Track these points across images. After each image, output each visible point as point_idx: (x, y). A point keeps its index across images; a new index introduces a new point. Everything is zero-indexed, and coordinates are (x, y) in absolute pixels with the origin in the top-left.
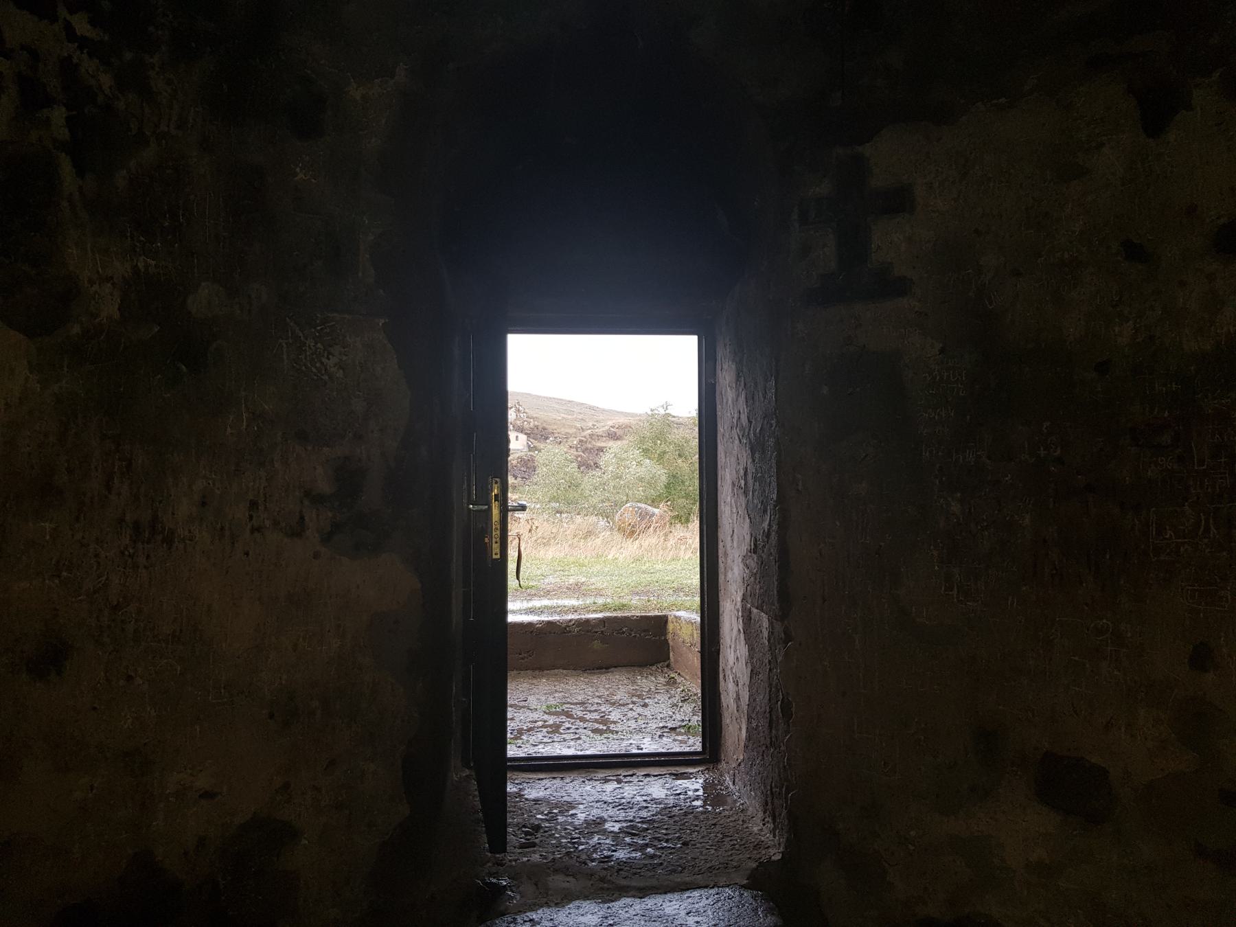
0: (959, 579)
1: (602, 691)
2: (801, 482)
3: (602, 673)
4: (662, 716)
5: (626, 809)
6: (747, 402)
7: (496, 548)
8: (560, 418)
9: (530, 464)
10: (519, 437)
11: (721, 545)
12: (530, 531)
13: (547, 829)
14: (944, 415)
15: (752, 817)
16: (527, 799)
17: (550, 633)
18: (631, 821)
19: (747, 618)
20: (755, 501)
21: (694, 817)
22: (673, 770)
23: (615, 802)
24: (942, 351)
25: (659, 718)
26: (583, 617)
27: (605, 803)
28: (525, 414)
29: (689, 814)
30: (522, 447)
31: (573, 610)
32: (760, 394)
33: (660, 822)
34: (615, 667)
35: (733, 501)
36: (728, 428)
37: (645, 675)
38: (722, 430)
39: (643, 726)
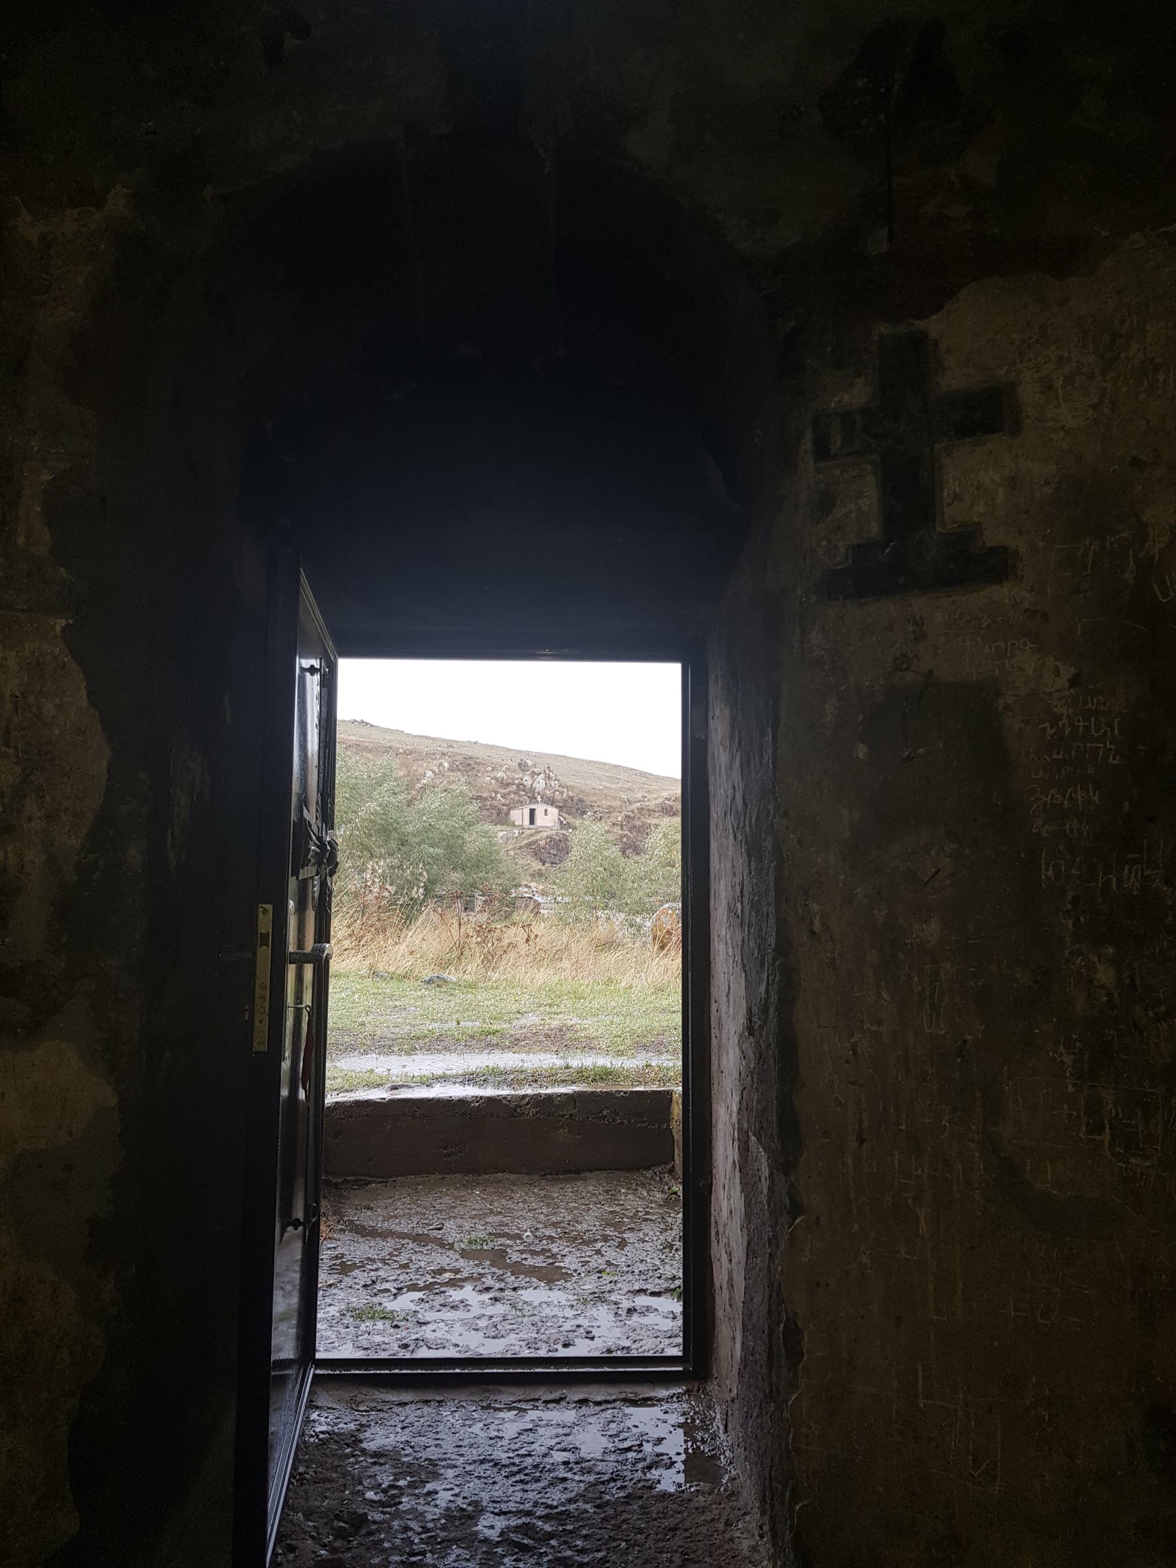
0: (1114, 1112)
1: (564, 1215)
2: (818, 917)
3: (569, 1181)
4: (642, 1267)
5: (527, 1483)
6: (742, 770)
7: (261, 1028)
8: (601, 787)
9: (562, 845)
10: (549, 812)
11: (714, 1007)
12: (527, 941)
13: (374, 1527)
14: (1080, 800)
15: (745, 1514)
16: (363, 1451)
17: (492, 1115)
18: (528, 1513)
19: (744, 1149)
20: (751, 944)
21: (641, 1507)
22: (629, 1391)
23: (514, 1464)
24: (1074, 682)
25: (637, 1272)
26: (542, 1091)
27: (496, 1464)
28: (557, 782)
29: (635, 1498)
30: (552, 824)
31: (531, 1078)
32: (757, 758)
33: (578, 1519)
34: (591, 1171)
35: (728, 936)
36: (721, 813)
37: (634, 1187)
38: (715, 816)
39: (608, 1287)
